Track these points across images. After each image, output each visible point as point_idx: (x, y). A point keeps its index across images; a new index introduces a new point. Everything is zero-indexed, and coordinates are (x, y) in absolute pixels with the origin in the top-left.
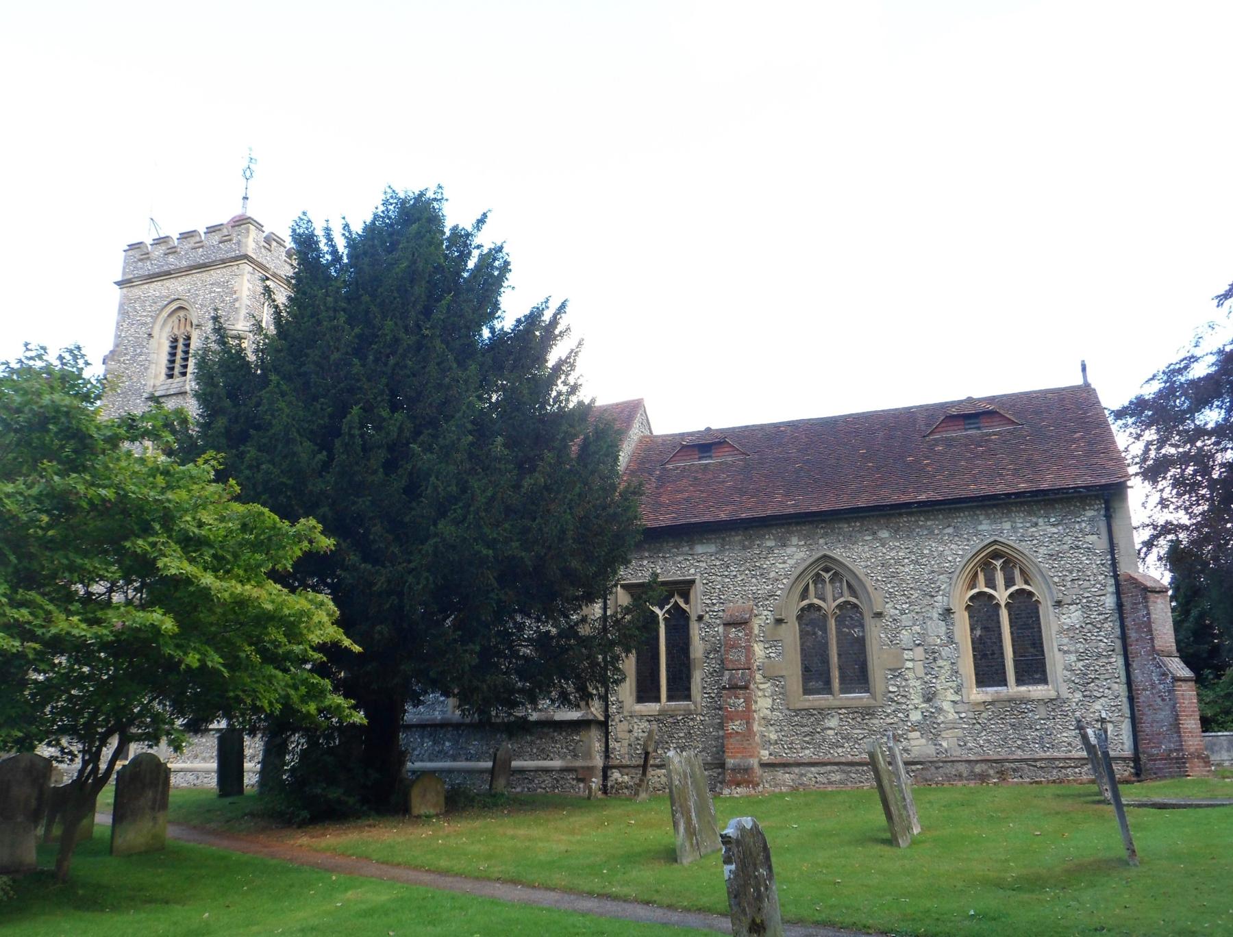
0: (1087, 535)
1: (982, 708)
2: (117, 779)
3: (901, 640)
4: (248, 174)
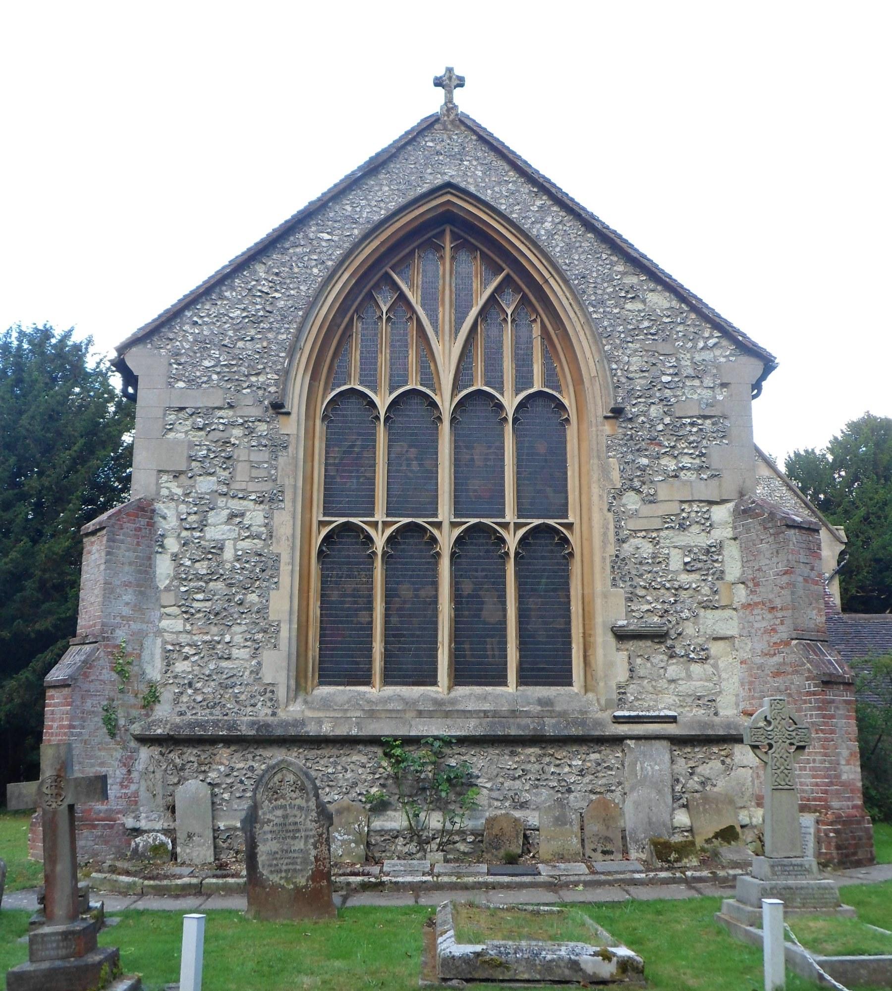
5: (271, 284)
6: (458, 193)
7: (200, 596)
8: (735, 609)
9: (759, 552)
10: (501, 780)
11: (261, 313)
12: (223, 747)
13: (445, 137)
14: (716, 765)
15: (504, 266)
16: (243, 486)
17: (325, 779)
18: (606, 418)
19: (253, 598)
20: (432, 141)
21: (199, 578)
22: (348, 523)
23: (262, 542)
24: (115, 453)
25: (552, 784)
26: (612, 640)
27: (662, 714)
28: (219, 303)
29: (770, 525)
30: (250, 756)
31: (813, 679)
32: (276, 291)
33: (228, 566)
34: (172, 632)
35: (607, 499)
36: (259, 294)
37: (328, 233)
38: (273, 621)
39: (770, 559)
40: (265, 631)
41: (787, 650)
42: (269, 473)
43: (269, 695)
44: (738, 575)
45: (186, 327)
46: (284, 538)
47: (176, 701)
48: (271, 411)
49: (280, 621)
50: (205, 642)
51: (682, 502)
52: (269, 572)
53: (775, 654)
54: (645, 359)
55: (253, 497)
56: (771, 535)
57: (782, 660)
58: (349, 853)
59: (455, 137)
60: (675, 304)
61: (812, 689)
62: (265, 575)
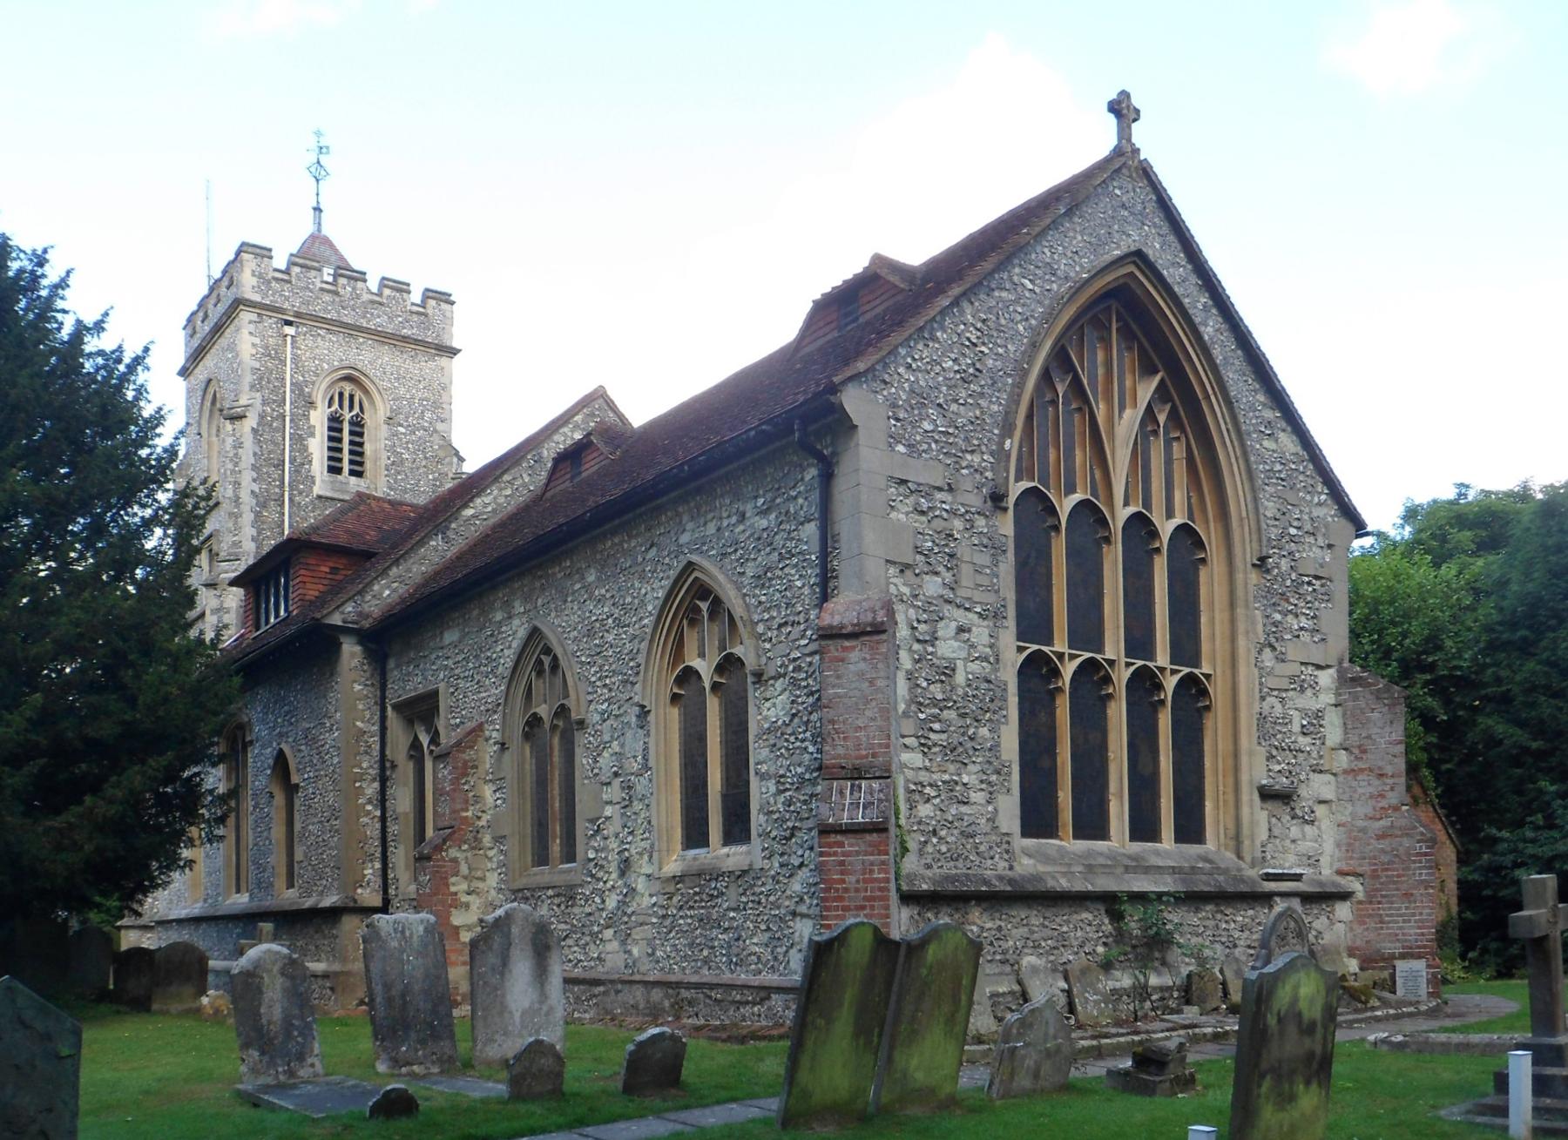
0: (802, 524)
1: (671, 889)
2: (658, 1034)
3: (601, 769)
4: (318, 173)
5: (979, 334)
6: (1143, 266)
7: (936, 726)
8: (1335, 775)
9: (1369, 720)
10: (1189, 936)
11: (971, 370)
12: (976, 905)
13: (1130, 186)
14: (1323, 919)
15: (1160, 366)
16: (968, 593)
17: (1060, 938)
18: (1254, 565)
19: (984, 731)
20: (1121, 188)
21: (935, 702)
22: (1092, 658)
23: (990, 666)
24: (28, 438)
25: (1223, 940)
27: (1292, 871)
28: (931, 345)
29: (1386, 696)
30: (997, 915)
31: (1426, 842)
32: (984, 344)
33: (960, 691)
34: (912, 769)
35: (1254, 653)
36: (967, 343)
37: (1030, 280)
38: (1005, 761)
39: (1382, 728)
40: (998, 773)
41: (1397, 814)
42: (992, 582)
43: (1005, 846)
44: (1338, 741)
45: (901, 370)
46: (1009, 664)
47: (921, 853)
48: (989, 503)
49: (1010, 761)
50: (944, 782)
51: (1302, 663)
52: (998, 703)
53: (1382, 818)
54: (1278, 506)
55: (978, 610)
56: (1385, 705)
57: (1389, 824)
58: (1101, 1013)
59: (1138, 190)
60: (1299, 449)
61: (1424, 850)
62: (993, 707)
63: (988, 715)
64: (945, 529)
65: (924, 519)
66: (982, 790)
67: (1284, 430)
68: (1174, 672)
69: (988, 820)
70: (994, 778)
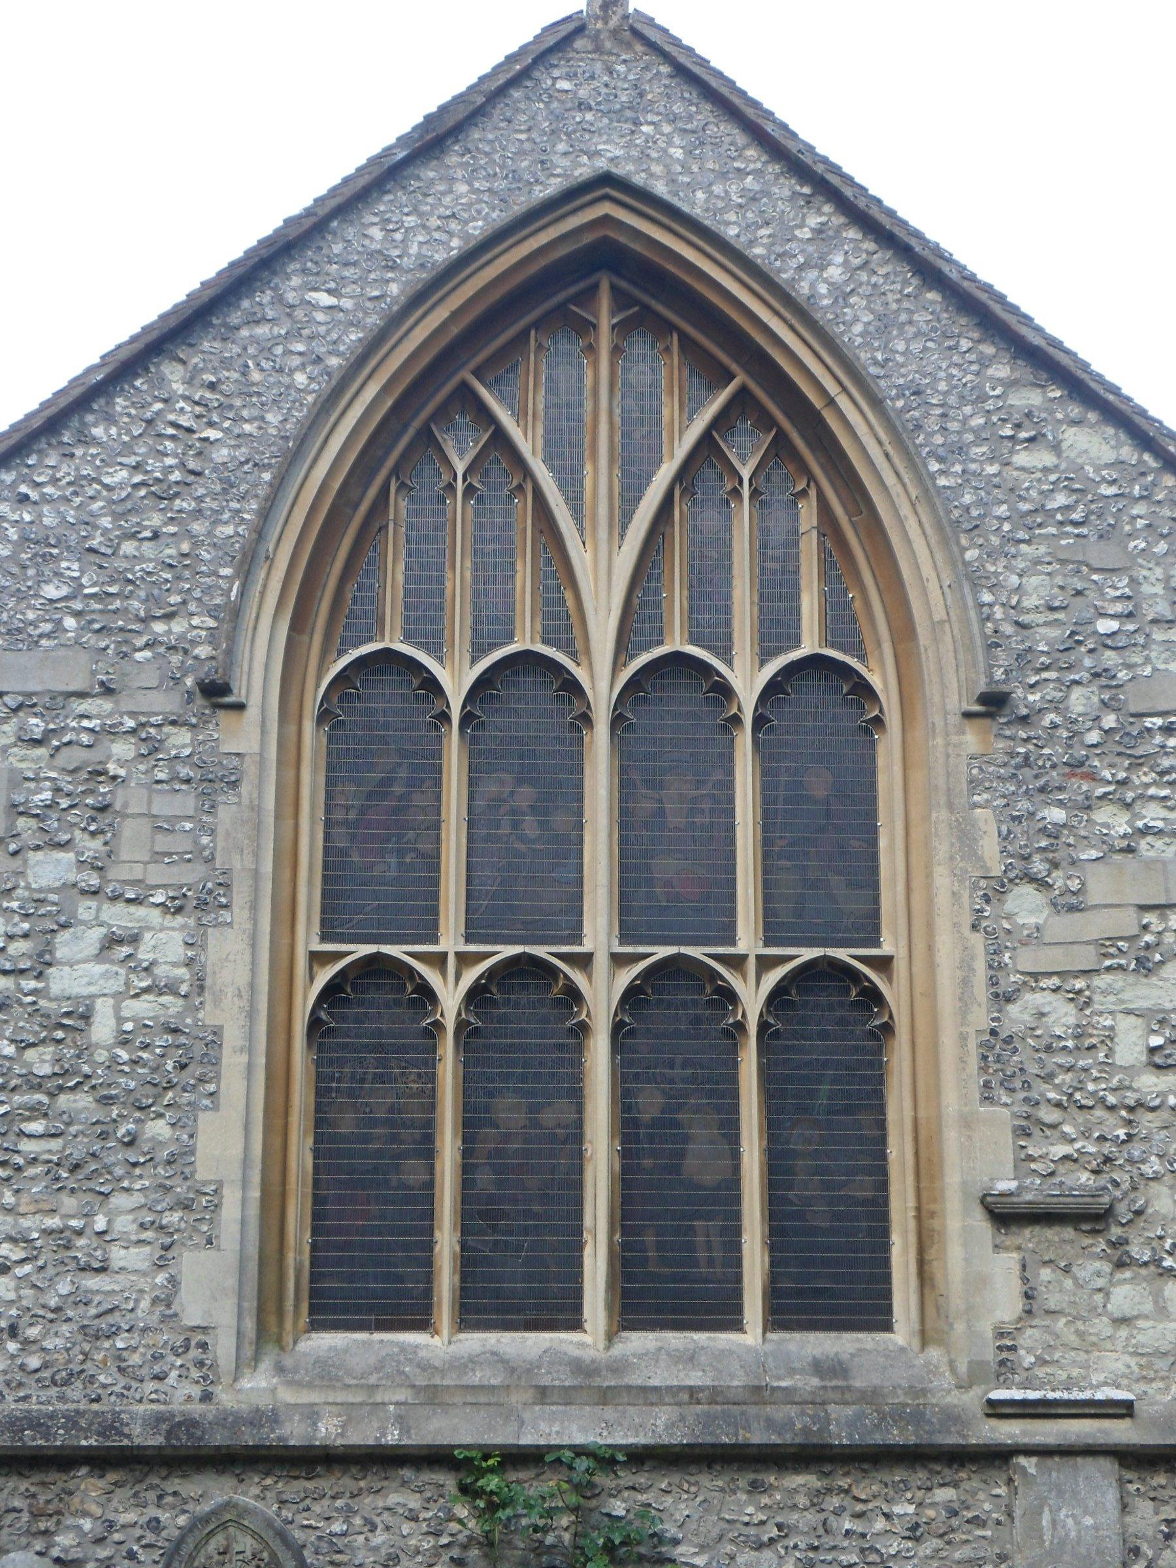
5: (198, 409)
7: (37, 1127)
11: (176, 476)
15: (734, 367)
17: (325, 1547)
18: (968, 715)
19: (158, 1129)
20: (568, 77)
26: (982, 1225)
28: (79, 452)
32: (211, 424)
33: (102, 1056)
43: (194, 1353)
48: (200, 701)
51: (1144, 908)
54: (1059, 580)
59: (621, 68)
60: (1128, 453)
62: (188, 1077)
63: (170, 1094)
64: (86, 763)
65: (41, 751)
66: (140, 1242)
67: (1075, 423)
68: (619, 961)
69: (155, 1301)
70: (173, 1218)
